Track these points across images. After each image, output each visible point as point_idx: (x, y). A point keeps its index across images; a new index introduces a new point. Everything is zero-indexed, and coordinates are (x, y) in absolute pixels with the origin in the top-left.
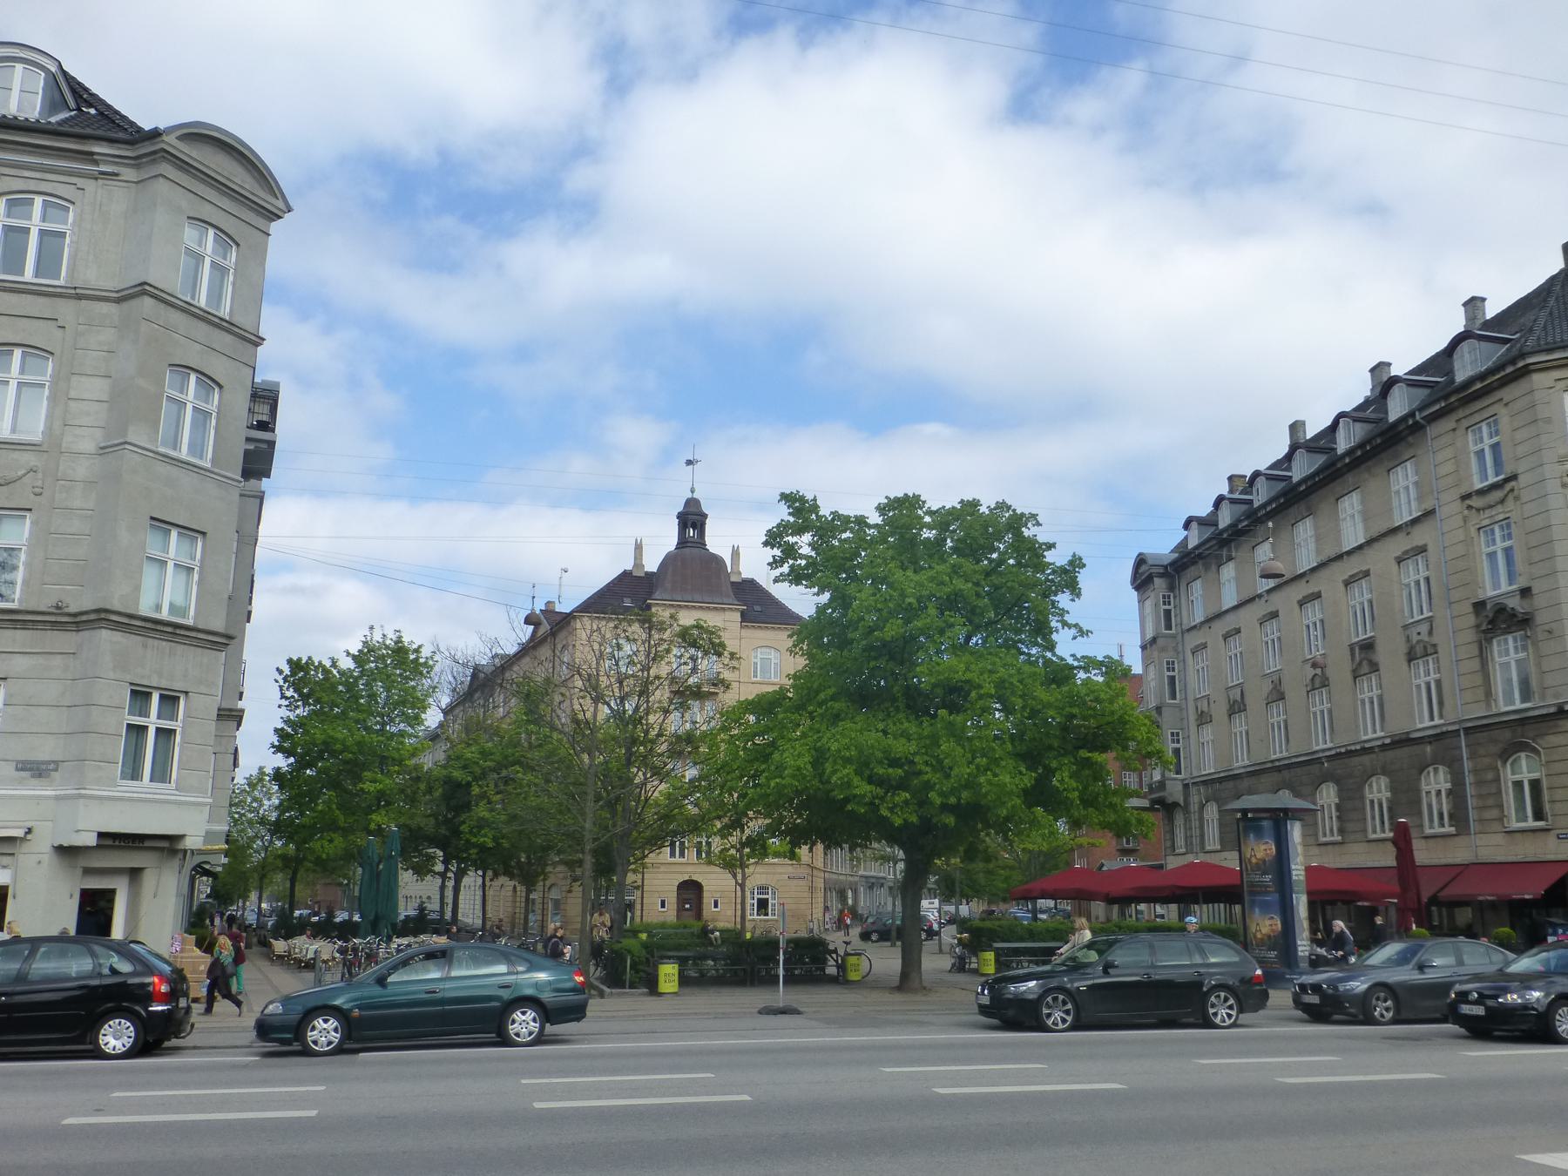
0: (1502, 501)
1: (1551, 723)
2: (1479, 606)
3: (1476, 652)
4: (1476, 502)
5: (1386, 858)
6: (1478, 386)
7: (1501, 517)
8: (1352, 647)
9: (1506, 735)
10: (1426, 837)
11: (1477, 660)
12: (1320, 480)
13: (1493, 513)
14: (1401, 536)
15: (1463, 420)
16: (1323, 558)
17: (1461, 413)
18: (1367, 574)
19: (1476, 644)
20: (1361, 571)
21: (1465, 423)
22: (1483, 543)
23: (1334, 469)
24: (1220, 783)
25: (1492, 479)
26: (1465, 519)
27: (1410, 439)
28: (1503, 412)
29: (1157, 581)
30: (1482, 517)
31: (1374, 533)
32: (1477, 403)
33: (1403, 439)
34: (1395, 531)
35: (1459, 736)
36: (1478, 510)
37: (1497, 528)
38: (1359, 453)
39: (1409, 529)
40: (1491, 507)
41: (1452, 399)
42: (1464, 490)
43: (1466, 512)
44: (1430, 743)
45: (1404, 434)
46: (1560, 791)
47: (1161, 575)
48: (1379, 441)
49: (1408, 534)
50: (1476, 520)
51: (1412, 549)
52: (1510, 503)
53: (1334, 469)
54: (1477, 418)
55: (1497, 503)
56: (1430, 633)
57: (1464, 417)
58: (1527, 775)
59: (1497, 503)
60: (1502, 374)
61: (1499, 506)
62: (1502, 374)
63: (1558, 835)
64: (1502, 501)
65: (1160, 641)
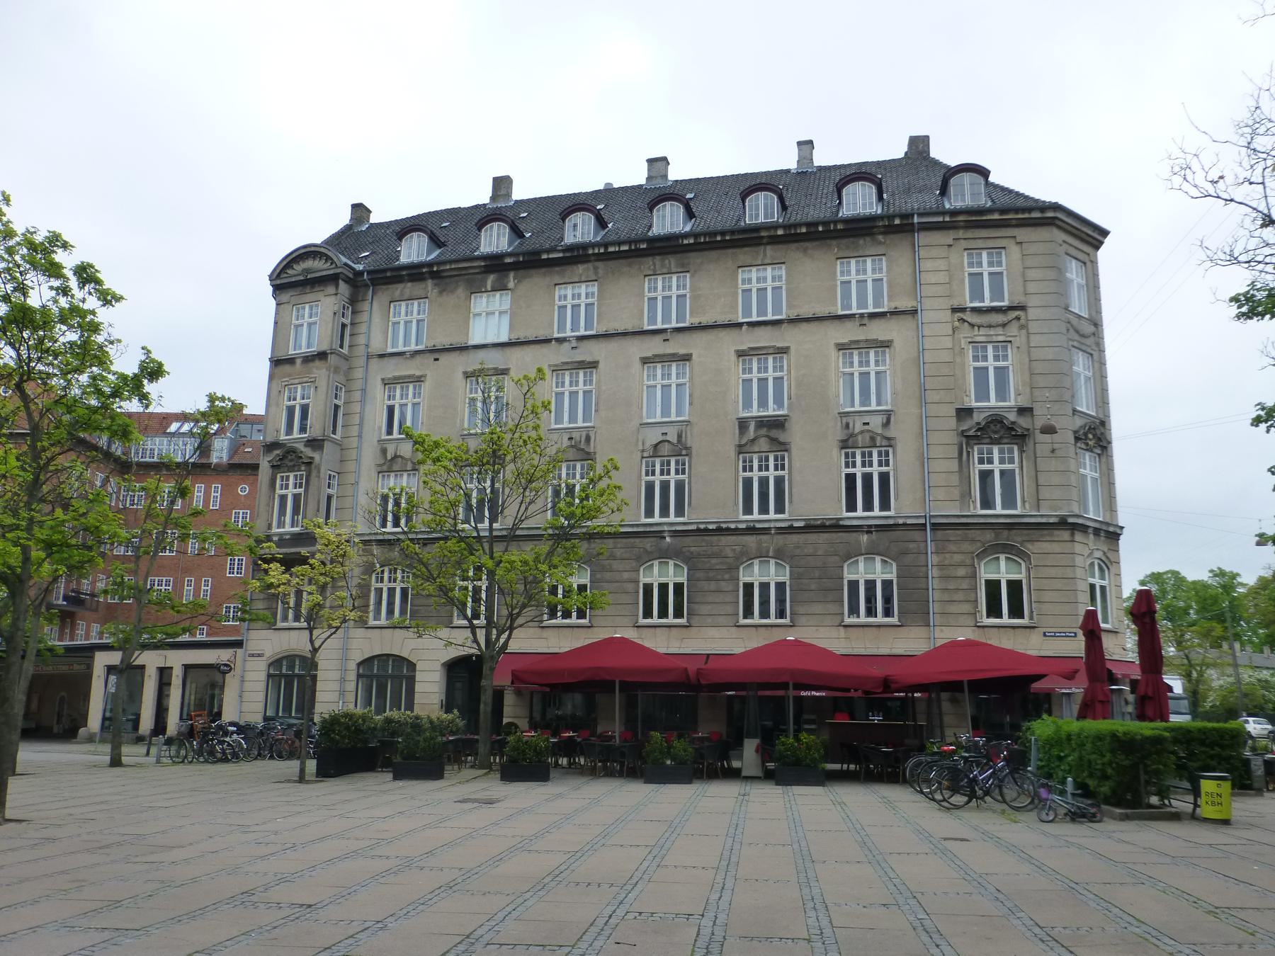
0: (1004, 325)
1: (1045, 532)
2: (964, 413)
3: (956, 455)
4: (968, 316)
5: (1076, 647)
6: (996, 216)
7: (1001, 338)
8: (743, 424)
9: (989, 536)
10: (846, 626)
11: (956, 462)
12: (705, 243)
13: (992, 333)
14: (658, 339)
15: (962, 241)
16: (514, 337)
17: (961, 234)
18: (687, 358)
19: (956, 447)
20: (773, 347)
21: (964, 244)
22: (286, 398)
23: (755, 235)
24: (425, 545)
25: (413, 347)
26: (954, 329)
27: (880, 238)
28: (1015, 250)
29: (342, 284)
30: (976, 333)
31: (523, 334)
32: (977, 230)
33: (871, 235)
34: (464, 349)
35: (926, 530)
36: (972, 325)
37: (990, 348)
38: (719, 238)
39: (865, 321)
40: (990, 326)
41: (961, 218)
42: (956, 304)
43: (957, 324)
44: (868, 532)
45: (765, 241)
46: (1050, 593)
47: (348, 281)
48: (804, 230)
49: (436, 360)
50: (965, 332)
51: (494, 369)
52: (1013, 329)
53: (755, 235)
54: (980, 244)
55: (998, 326)
56: (887, 424)
57: (965, 239)
58: (1005, 575)
59: (998, 326)
60: (1026, 215)
61: (1001, 328)
62: (1026, 215)
63: (1044, 633)
64: (1004, 325)
65: (332, 359)
